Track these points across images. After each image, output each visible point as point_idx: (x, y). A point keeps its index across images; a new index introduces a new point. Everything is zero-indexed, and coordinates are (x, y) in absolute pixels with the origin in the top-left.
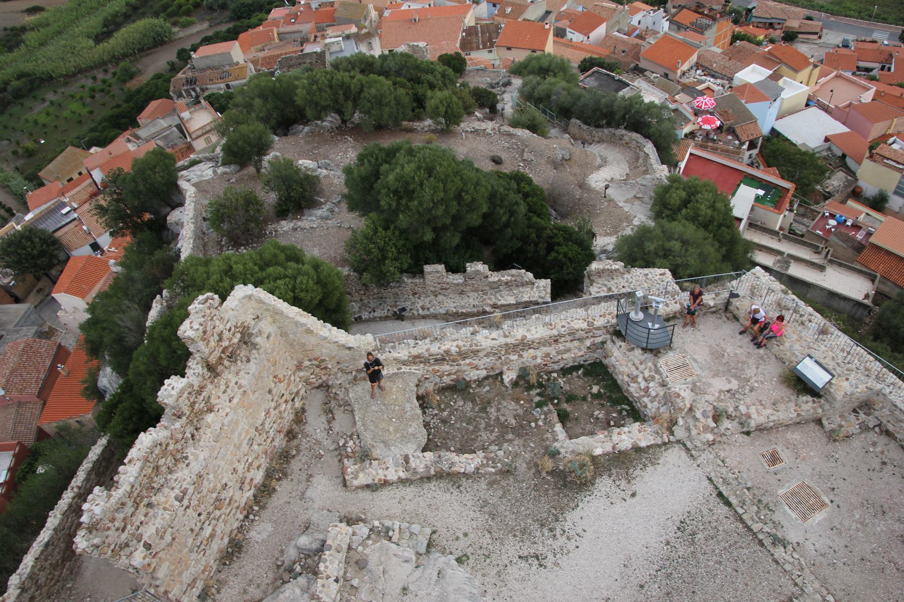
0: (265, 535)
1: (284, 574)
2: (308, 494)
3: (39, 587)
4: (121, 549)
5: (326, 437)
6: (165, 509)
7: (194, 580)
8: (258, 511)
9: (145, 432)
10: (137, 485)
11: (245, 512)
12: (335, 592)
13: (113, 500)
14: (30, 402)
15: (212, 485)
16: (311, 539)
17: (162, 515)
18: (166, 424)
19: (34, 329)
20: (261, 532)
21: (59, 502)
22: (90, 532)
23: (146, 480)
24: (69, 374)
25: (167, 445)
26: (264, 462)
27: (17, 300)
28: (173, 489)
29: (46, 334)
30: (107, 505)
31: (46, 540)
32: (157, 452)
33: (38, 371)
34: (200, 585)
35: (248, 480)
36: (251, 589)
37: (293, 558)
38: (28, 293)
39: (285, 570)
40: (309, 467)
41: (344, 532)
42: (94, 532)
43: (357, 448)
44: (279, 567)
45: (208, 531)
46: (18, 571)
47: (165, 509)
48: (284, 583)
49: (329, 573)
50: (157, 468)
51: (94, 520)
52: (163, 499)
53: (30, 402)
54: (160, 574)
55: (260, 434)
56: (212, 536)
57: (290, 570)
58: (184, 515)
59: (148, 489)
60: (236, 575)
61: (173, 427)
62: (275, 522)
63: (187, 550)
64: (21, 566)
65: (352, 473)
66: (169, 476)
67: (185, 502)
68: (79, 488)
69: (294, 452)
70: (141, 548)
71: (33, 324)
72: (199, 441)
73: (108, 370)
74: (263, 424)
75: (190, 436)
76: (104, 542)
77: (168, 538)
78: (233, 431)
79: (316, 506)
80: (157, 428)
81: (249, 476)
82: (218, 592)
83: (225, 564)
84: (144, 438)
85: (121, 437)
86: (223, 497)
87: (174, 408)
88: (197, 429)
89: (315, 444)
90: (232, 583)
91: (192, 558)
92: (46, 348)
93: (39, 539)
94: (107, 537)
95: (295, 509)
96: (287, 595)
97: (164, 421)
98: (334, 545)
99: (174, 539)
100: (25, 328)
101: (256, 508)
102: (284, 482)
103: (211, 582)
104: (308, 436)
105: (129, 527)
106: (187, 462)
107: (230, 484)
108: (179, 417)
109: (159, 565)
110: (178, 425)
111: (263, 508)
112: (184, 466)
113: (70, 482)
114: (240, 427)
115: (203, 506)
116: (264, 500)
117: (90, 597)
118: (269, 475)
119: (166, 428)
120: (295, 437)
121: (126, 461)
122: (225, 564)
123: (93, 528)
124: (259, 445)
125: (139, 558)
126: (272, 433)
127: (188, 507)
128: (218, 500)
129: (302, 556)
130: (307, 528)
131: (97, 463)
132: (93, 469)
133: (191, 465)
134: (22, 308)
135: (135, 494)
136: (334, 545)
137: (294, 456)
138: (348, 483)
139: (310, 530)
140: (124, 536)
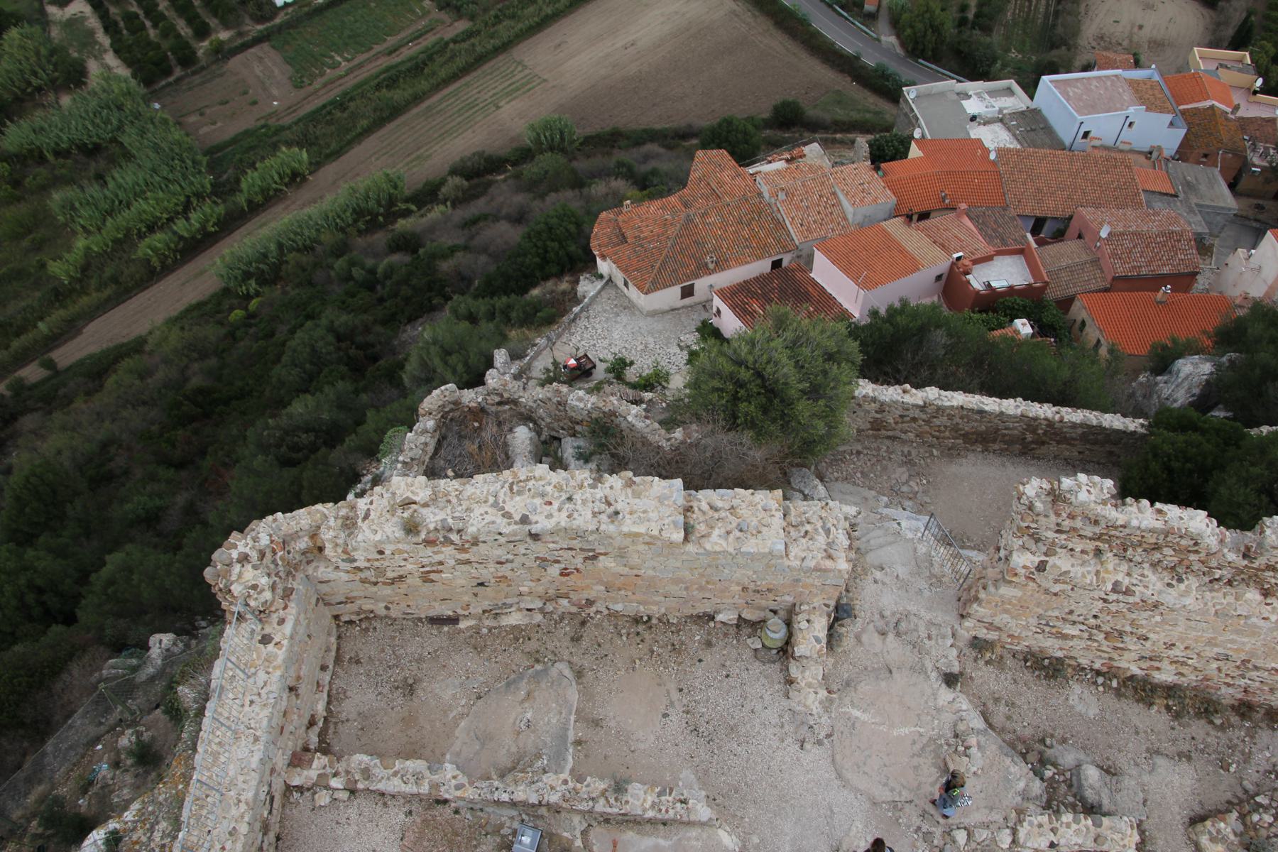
0: (1080, 708)
1: (1035, 753)
2: (1160, 761)
3: (927, 422)
4: (1031, 536)
5: (1261, 769)
6: (1097, 573)
7: (999, 629)
8: (1110, 687)
9: (1209, 516)
10: (1127, 531)
11: (1105, 669)
12: (1036, 846)
13: (1099, 508)
14: (1102, 272)
15: (1144, 622)
16: (1097, 785)
17: (1089, 572)
18: (1228, 540)
19: (1202, 229)
20: (1082, 700)
21: (1036, 404)
22: (1049, 494)
23: (1135, 539)
24: (1161, 303)
25: (1197, 552)
26: (1191, 678)
27: (1232, 186)
28: (1129, 574)
29: (1204, 249)
30: (1092, 505)
31: (987, 408)
32: (1183, 542)
33: (1149, 263)
34: (992, 636)
35: (1156, 664)
36: (1002, 709)
37: (1060, 761)
38: (1249, 194)
39: (1041, 753)
40: (1202, 751)
41: (1126, 842)
42: (1049, 499)
43: (1263, 833)
44: (1042, 741)
45: (1070, 630)
46: (942, 392)
47: (1097, 573)
48: (1024, 756)
49: (1062, 830)
50: (1157, 547)
51: (1068, 496)
52: (1110, 567)
53: (1102, 272)
54: (1005, 591)
55: (1238, 667)
56: (1065, 637)
57: (1043, 762)
58: (1093, 599)
59: (1123, 544)
60: (1015, 681)
61: (1226, 551)
62: (1103, 718)
63: (1041, 612)
64: (949, 393)
65: (1219, 831)
66: (1146, 565)
67: (1113, 597)
68: (1061, 421)
69: (1218, 722)
70: (1037, 559)
71: (1209, 224)
72: (1211, 590)
73: (1207, 368)
74: (1256, 668)
75: (1217, 576)
76: (1038, 515)
77: (1057, 588)
78: (1238, 632)
79: (1146, 778)
80: (1217, 530)
81: (1165, 665)
82: (987, 663)
83: (1026, 661)
84: (1198, 519)
85: (1155, 455)
86: (1126, 639)
87: (1260, 545)
88: (1230, 583)
89: (1243, 753)
90: (1003, 677)
91: (1031, 620)
92: (1187, 256)
93: (986, 400)
94: (1046, 516)
95: (1131, 745)
96: (1012, 770)
97: (1229, 535)
98: (1103, 830)
99: (1056, 594)
100: (1199, 218)
101: (1115, 684)
102: (1166, 717)
103: (998, 650)
104: (1252, 737)
105: (1064, 536)
106: (1174, 582)
107: (1148, 644)
108: (1245, 556)
109: (1016, 585)
110: (1231, 557)
111: (1118, 693)
112: (1167, 580)
113: (1063, 406)
114: (1246, 640)
115: (1109, 618)
116: (1129, 693)
117: (928, 482)
118: (1171, 691)
119: (1222, 541)
120: (1243, 716)
121: (1158, 505)
122: (1026, 661)
123: (1056, 497)
124: (1219, 669)
125: (1023, 560)
126: (1242, 682)
127: (1105, 601)
128: (1121, 634)
129: (1068, 775)
130: (1108, 772)
131: (1100, 429)
132: (1091, 427)
133: (1170, 590)
134: (1227, 199)
135: (1112, 533)
136: (1103, 830)
137: (1211, 722)
138: (1199, 827)
139: (1108, 778)
140: (1050, 534)
